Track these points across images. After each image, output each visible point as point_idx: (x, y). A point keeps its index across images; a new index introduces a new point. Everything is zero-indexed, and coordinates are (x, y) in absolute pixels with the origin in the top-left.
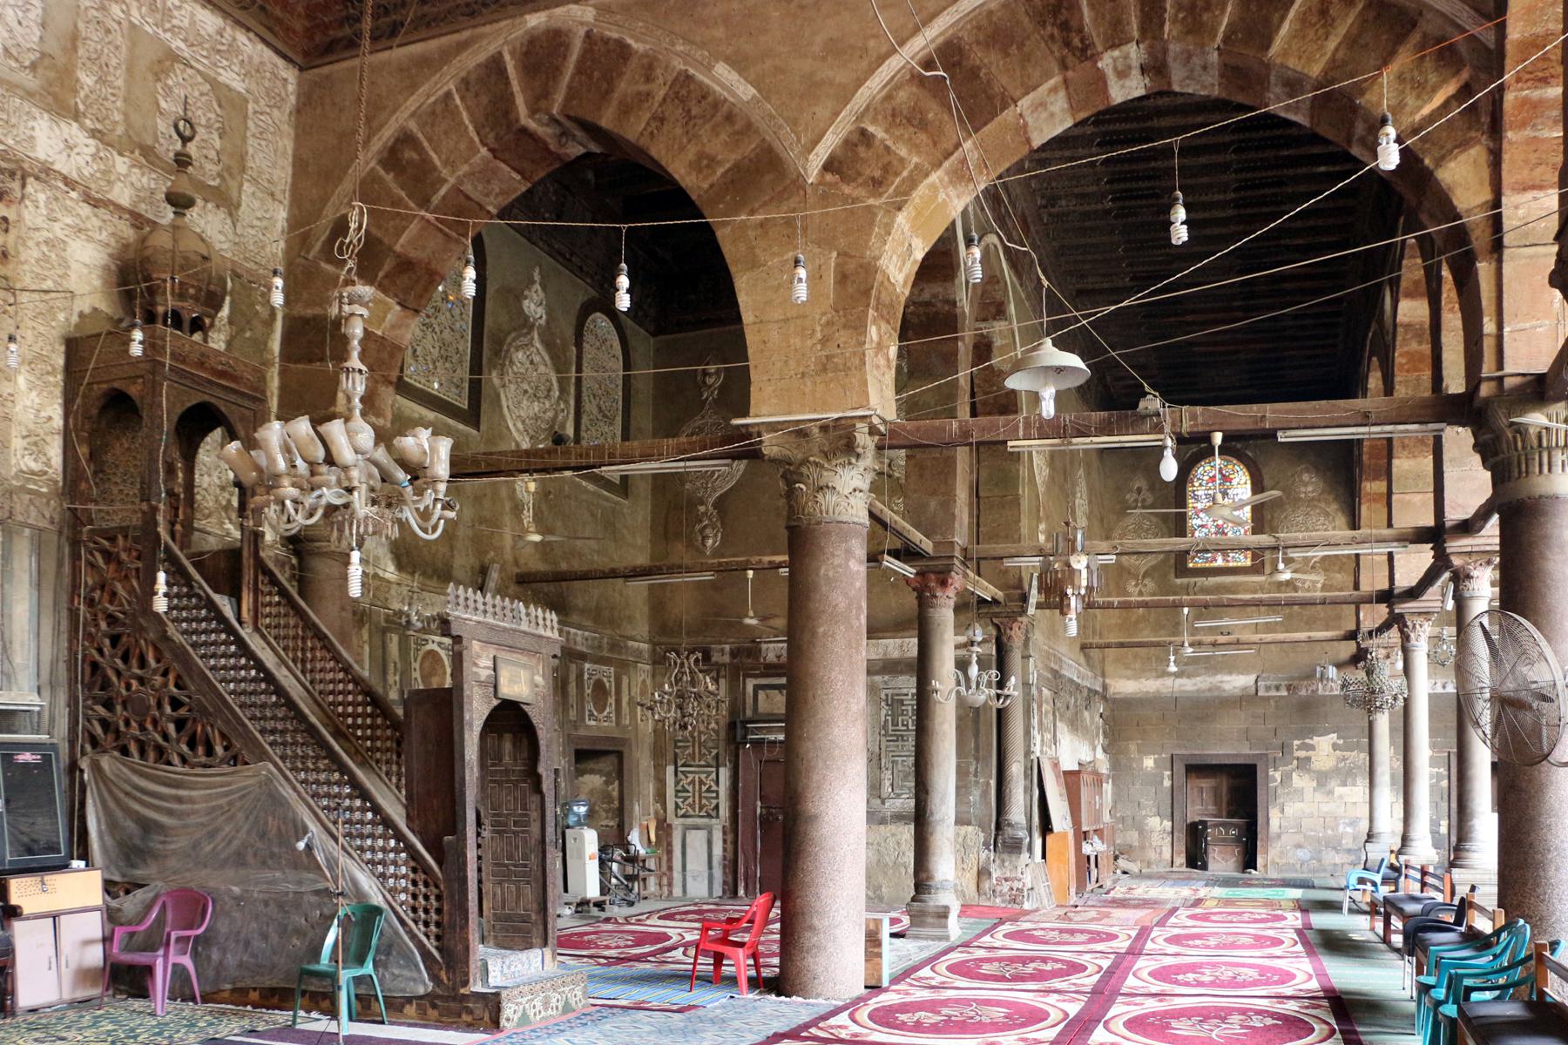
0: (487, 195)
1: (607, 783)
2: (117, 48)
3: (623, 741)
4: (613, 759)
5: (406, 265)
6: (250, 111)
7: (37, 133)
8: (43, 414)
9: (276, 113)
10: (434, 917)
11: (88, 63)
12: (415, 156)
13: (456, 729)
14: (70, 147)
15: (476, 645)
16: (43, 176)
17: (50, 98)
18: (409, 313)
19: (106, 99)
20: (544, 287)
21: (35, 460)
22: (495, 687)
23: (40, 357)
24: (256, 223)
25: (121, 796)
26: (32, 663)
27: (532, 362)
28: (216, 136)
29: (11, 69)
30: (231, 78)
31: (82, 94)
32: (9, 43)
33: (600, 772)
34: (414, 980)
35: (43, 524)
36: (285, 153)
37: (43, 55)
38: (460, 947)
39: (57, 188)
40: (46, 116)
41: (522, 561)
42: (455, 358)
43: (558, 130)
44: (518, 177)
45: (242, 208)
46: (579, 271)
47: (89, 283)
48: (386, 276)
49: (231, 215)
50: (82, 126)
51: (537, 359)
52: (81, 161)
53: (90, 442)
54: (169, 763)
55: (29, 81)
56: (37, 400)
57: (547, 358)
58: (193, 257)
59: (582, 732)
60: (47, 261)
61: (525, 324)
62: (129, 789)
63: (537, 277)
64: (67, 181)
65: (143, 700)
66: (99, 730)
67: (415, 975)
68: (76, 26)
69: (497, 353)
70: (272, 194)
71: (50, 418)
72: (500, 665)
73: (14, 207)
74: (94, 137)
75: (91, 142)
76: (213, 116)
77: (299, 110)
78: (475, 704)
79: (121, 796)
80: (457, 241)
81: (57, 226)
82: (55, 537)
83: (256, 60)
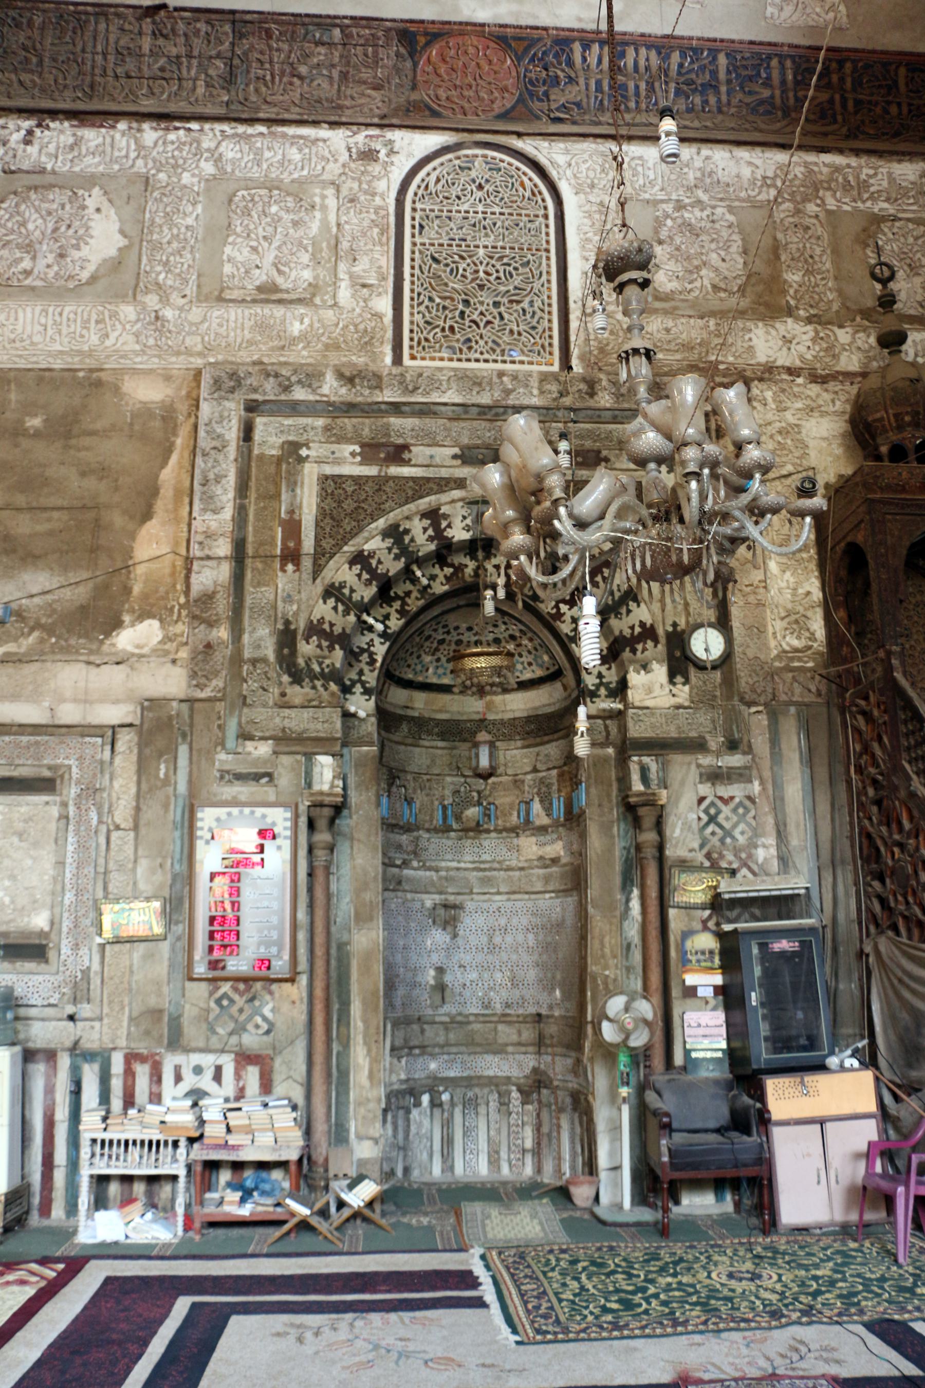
2: (818, 238)
7: (755, 341)
8: (800, 591)
11: (793, 264)
14: (787, 341)
16: (767, 375)
17: (762, 309)
19: (817, 285)
21: (799, 638)
25: (895, 982)
26: (810, 844)
29: (721, 300)
31: (792, 292)
35: (810, 698)
39: (782, 381)
40: (760, 324)
50: (797, 319)
52: (802, 349)
56: (792, 580)
58: (900, 384)
62: (900, 974)
64: (790, 371)
65: (902, 868)
66: (877, 907)
68: (775, 239)
71: (808, 593)
74: (810, 323)
75: (809, 328)
79: (895, 982)
82: (825, 709)
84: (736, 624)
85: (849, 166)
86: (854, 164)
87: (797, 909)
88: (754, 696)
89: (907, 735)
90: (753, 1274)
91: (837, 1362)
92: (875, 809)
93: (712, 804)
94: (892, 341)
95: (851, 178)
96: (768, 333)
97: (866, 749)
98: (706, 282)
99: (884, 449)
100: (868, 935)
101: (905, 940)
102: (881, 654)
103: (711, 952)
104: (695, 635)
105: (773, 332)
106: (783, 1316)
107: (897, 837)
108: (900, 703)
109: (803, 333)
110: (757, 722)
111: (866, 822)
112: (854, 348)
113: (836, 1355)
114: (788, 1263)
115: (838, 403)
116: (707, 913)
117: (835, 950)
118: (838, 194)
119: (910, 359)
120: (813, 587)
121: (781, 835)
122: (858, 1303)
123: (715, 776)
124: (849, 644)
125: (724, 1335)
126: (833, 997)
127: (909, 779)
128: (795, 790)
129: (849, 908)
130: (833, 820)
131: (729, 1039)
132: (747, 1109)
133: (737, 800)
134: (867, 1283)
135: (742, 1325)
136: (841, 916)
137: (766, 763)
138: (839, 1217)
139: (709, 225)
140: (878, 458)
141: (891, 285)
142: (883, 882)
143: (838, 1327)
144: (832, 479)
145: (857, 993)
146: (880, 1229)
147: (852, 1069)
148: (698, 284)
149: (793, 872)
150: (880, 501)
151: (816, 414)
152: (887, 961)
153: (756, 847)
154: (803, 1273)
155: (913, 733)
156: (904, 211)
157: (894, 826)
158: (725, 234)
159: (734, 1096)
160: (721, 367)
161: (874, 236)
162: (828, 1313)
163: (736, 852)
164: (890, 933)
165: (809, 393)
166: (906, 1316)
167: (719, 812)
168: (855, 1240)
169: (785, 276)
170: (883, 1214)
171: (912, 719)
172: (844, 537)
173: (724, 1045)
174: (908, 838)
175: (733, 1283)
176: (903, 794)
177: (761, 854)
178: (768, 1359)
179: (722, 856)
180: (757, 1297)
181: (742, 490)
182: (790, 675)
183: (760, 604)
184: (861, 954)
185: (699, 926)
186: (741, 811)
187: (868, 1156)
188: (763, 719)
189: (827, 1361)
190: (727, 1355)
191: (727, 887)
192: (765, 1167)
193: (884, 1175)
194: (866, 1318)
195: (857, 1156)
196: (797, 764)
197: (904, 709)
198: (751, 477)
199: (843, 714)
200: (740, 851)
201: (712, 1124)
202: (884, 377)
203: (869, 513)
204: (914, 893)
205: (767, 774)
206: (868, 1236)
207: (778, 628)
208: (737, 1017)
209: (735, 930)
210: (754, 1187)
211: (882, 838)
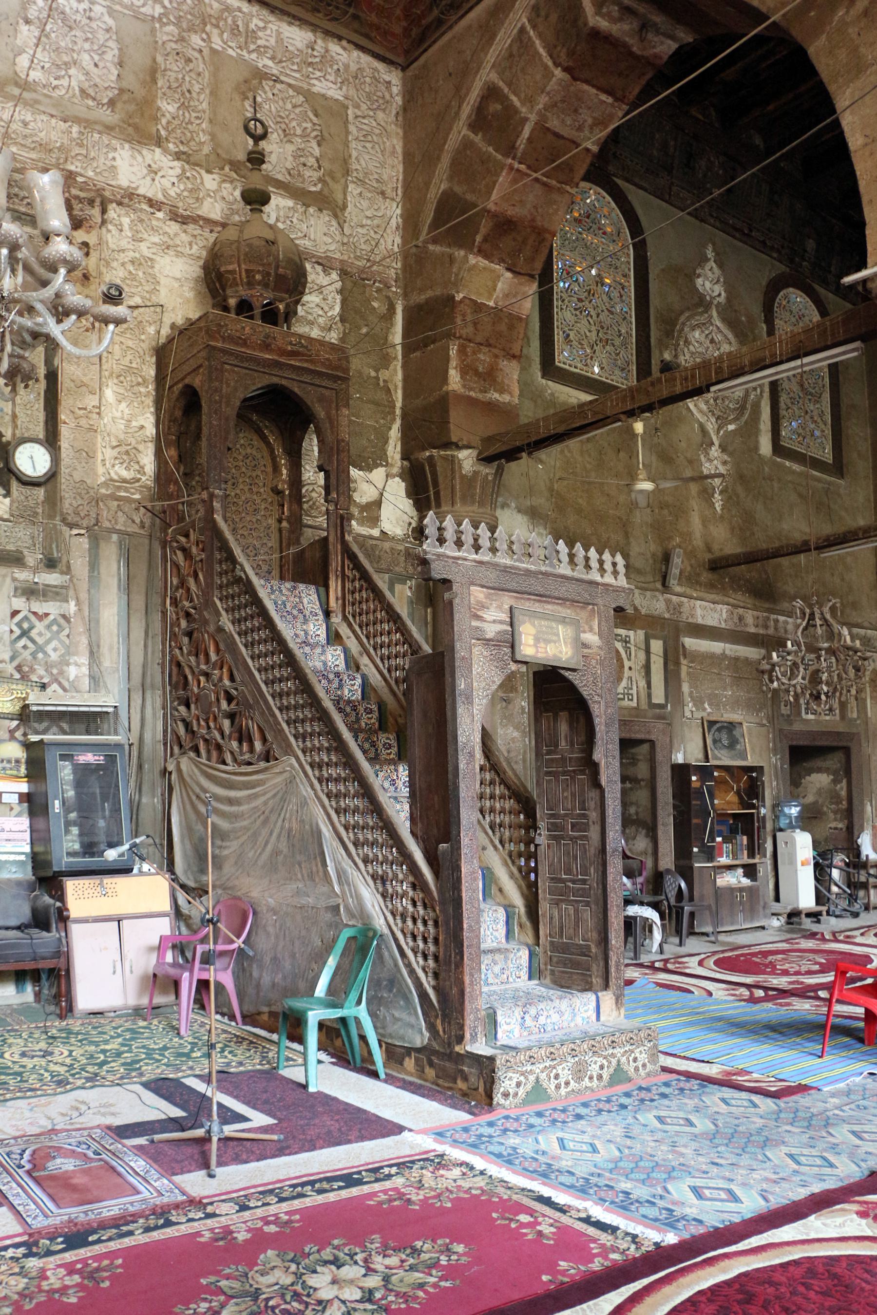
0: (580, 129)
1: (835, 781)
2: (199, 74)
3: (851, 736)
4: (840, 755)
5: (505, 226)
6: (351, 117)
7: (118, 163)
8: (134, 424)
9: (380, 115)
10: (432, 948)
12: (499, 107)
13: (449, 703)
14: (152, 171)
15: (478, 593)
16: (126, 201)
17: (130, 130)
18: (524, 279)
20: (721, 266)
21: (127, 469)
22: (513, 647)
23: (129, 370)
24: (369, 222)
27: (712, 341)
28: (314, 144)
30: (327, 87)
31: (164, 121)
32: (86, 85)
33: (827, 771)
34: (412, 1026)
35: (133, 529)
36: (393, 153)
37: (122, 91)
38: (454, 991)
39: (141, 210)
40: (127, 146)
41: (716, 547)
42: (617, 342)
43: (636, 25)
44: (610, 100)
45: (349, 209)
46: (763, 247)
47: (181, 296)
48: (485, 240)
49: (336, 216)
50: (166, 151)
51: (719, 337)
53: (178, 444)
54: (224, 763)
55: (106, 115)
56: (127, 411)
57: (731, 336)
58: (257, 243)
59: (797, 727)
60: (134, 279)
61: (702, 303)
62: (198, 790)
63: (710, 254)
64: (151, 202)
65: (206, 694)
66: (182, 730)
67: (412, 1020)
68: (154, 60)
69: (669, 334)
70: (383, 193)
71: (142, 427)
72: (516, 613)
73: (94, 233)
74: (178, 159)
75: (176, 164)
76: (309, 125)
77: (405, 109)
78: (476, 669)
79: (194, 798)
80: (561, 191)
81: (143, 246)
82: (147, 541)
83: (353, 67)
84: (64, 443)
85: (239, 10)
86: (245, 10)
87: (106, 726)
88: (77, 519)
89: (221, 574)
90: (46, 1051)
91: (113, 1114)
92: (186, 640)
93: (26, 618)
94: (256, 199)
95: (240, 23)
96: (133, 157)
97: (182, 584)
98: (74, 83)
99: (232, 302)
100: (172, 755)
101: (204, 761)
102: (205, 495)
103: (18, 761)
104: (21, 449)
105: (139, 158)
106: (68, 1083)
107: (203, 667)
108: (217, 544)
109: (171, 168)
110: (78, 547)
111: (177, 651)
112: (218, 196)
113: (112, 1109)
114: (80, 1041)
115: (195, 247)
116: (15, 723)
117: (140, 767)
118: (225, 35)
119: (272, 221)
120: (148, 422)
121: (94, 654)
122: (140, 1068)
123: (30, 592)
124: (176, 482)
125: (9, 1104)
126: (135, 809)
127: (218, 614)
128: (111, 613)
129: (155, 730)
130: (146, 646)
131: (32, 843)
132: (47, 908)
133: (51, 617)
134: (149, 1054)
135: (29, 1094)
136: (148, 736)
137: (83, 586)
138: (132, 1001)
139: (85, 21)
140: (226, 309)
141: (263, 144)
142: (188, 706)
143: (118, 1088)
144: (180, 321)
145: (159, 807)
146: (169, 1010)
147: (149, 874)
148: (65, 82)
149: (103, 692)
150: (223, 351)
151: (172, 253)
152: (188, 779)
153: (68, 664)
154: (93, 1048)
155: (226, 573)
156: (287, 75)
157: (202, 657)
158: (101, 36)
159: (36, 896)
160: (80, 179)
161: (254, 90)
162: (110, 1077)
163: (48, 667)
164: (192, 754)
165: (167, 229)
166: (180, 1074)
167: (32, 628)
168: (145, 1020)
169: (159, 103)
170: (172, 997)
171: (227, 560)
172: (183, 379)
173: (27, 849)
174: (214, 669)
175: (25, 1061)
176: (212, 628)
177: (72, 672)
178: (49, 1118)
179: (32, 670)
180: (47, 1071)
181: (45, 284)
182: (116, 503)
183: (92, 430)
184: (165, 772)
185: (7, 736)
186: (55, 628)
187: (160, 949)
188: (85, 542)
189: (104, 1115)
190: (10, 1119)
191: (36, 699)
192: (63, 960)
193: (175, 965)
194: (144, 1079)
195: (151, 949)
196: (115, 589)
197: (220, 549)
198: (55, 271)
199: (164, 548)
200: (52, 667)
201: (14, 922)
202: (241, 231)
203: (208, 359)
204: (215, 719)
205: (84, 596)
206: (157, 1016)
207: (107, 457)
208: (41, 824)
209: (42, 741)
210: (52, 978)
211: (191, 667)
